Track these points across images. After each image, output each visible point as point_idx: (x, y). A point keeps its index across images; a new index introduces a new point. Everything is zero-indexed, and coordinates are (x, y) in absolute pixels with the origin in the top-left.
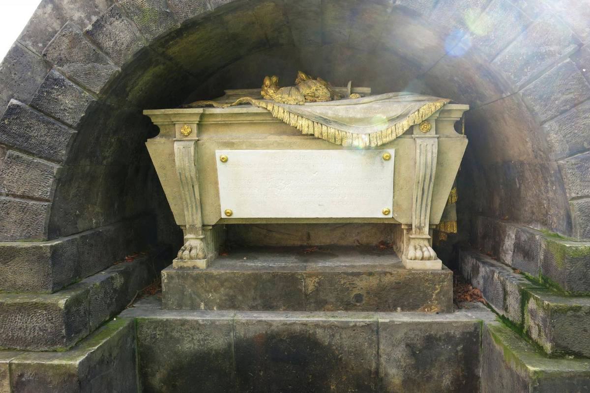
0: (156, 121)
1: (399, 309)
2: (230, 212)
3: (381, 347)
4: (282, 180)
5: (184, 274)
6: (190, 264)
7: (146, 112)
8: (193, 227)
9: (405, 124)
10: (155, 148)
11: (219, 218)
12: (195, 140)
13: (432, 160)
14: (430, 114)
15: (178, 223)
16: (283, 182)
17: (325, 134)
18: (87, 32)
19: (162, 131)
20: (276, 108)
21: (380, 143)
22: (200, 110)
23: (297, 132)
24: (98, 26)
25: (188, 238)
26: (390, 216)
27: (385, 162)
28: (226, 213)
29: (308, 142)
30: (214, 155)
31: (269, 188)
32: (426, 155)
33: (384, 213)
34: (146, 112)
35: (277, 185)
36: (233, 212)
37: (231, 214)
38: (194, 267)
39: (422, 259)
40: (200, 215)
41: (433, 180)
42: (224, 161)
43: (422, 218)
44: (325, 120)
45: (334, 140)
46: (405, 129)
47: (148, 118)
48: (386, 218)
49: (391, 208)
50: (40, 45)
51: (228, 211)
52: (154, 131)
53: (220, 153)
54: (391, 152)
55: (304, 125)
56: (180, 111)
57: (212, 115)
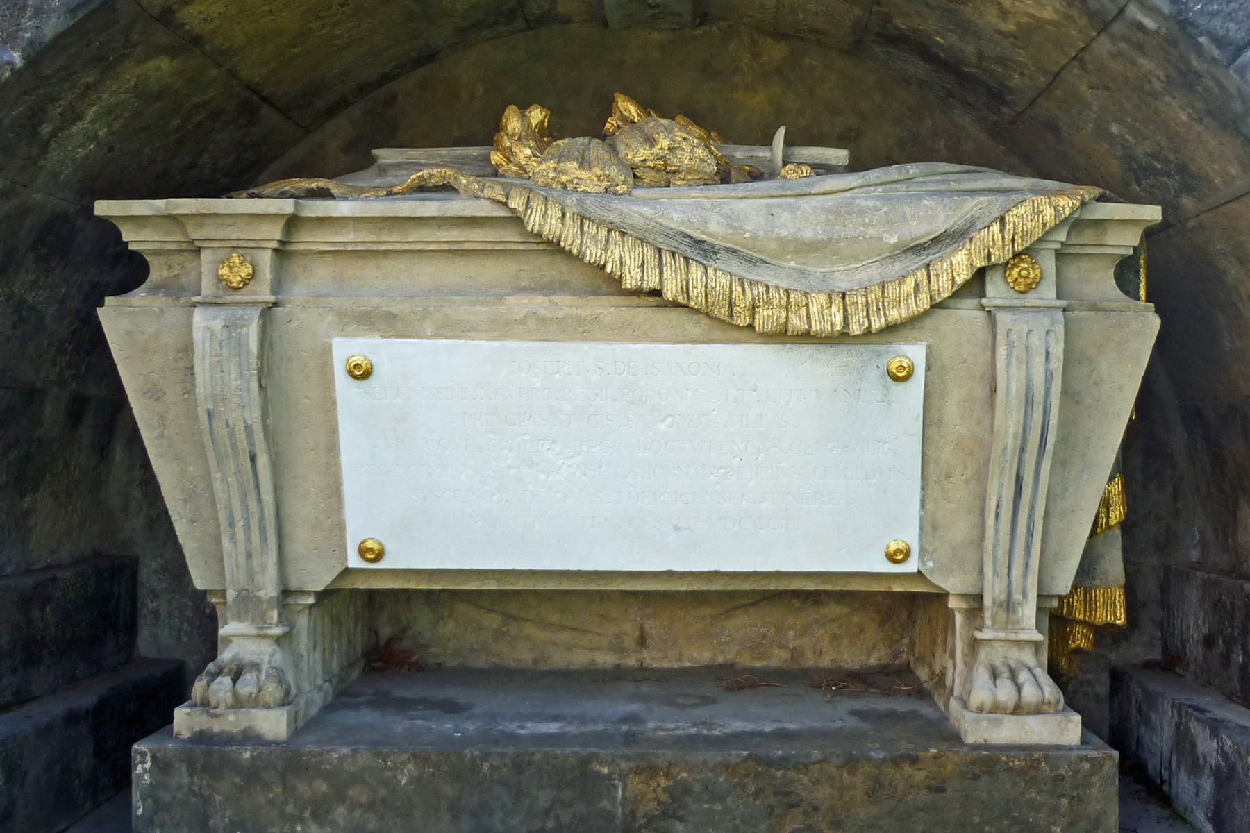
2: (376, 547)
4: (554, 442)
6: (231, 722)
7: (103, 208)
9: (961, 263)
17: (697, 291)
19: (157, 273)
21: (877, 324)
23: (613, 285)
26: (911, 566)
28: (362, 552)
30: (327, 352)
31: (510, 467)
33: (891, 558)
34: (103, 208)
36: (388, 548)
38: (249, 737)
42: (361, 373)
45: (725, 311)
47: (109, 228)
51: (369, 544)
54: (914, 352)
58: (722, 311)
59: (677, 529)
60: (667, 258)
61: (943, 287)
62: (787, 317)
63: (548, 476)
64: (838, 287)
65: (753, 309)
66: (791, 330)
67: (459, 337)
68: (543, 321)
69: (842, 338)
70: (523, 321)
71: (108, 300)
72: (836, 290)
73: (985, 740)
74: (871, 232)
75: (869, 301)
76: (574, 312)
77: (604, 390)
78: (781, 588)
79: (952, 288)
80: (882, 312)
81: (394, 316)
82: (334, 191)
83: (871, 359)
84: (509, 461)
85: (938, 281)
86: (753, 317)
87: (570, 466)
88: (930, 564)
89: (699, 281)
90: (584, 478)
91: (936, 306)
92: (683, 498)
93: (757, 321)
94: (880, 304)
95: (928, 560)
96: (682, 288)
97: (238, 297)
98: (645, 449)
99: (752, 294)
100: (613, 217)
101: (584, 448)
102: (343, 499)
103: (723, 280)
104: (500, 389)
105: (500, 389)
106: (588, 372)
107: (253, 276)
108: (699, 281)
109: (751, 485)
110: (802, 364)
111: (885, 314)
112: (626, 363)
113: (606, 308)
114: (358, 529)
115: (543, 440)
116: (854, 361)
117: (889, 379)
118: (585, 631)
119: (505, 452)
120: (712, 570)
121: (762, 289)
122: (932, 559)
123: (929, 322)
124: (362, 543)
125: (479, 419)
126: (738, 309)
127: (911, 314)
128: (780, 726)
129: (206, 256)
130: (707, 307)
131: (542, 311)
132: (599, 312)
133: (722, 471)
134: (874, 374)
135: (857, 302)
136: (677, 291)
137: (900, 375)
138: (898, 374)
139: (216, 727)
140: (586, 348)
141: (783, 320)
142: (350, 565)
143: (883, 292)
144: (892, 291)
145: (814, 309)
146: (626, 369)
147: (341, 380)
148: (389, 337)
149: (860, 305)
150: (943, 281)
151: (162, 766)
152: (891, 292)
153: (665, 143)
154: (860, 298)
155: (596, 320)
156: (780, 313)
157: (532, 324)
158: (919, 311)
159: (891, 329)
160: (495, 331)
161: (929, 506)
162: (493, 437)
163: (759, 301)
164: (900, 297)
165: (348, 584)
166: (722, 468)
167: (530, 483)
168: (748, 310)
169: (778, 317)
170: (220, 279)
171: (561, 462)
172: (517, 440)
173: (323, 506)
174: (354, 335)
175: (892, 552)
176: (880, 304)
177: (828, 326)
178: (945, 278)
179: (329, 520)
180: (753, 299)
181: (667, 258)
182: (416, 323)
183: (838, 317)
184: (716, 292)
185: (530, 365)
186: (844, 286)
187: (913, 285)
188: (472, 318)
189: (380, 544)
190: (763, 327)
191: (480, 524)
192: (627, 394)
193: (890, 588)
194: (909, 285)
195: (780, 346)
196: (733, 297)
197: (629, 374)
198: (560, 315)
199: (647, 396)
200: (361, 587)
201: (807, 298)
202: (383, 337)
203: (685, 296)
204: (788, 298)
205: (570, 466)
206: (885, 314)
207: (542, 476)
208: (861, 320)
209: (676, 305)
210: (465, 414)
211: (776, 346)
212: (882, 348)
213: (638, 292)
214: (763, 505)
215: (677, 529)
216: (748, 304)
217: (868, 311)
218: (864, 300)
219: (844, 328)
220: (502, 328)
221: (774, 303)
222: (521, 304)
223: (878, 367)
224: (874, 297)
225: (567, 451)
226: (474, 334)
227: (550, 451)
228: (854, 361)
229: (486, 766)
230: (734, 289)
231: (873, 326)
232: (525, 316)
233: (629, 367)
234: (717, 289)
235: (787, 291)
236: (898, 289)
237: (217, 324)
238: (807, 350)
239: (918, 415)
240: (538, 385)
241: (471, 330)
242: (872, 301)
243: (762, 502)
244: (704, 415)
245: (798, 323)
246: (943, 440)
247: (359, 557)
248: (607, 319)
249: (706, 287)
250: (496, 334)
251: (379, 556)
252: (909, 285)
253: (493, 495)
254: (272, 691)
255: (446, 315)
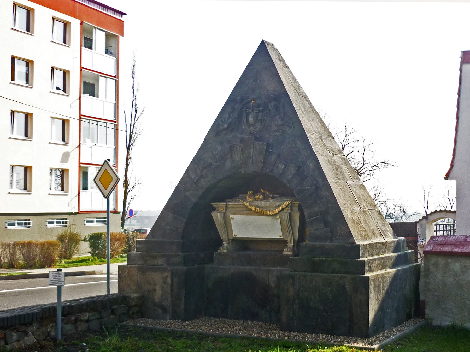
0: (215, 206)
1: (279, 266)
3: (270, 276)
5: (220, 254)
6: (222, 251)
7: (212, 203)
8: (225, 240)
9: (280, 208)
10: (214, 214)
12: (287, 206)
13: (288, 218)
14: (287, 205)
15: (222, 239)
17: (259, 211)
18: (195, 182)
19: (216, 209)
20: (246, 203)
21: (274, 214)
22: (225, 203)
23: (251, 210)
24: (198, 180)
25: (398, 322)
26: (282, 237)
27: (277, 220)
28: (235, 235)
34: (212, 203)
38: (223, 252)
39: (287, 251)
40: (227, 235)
42: (233, 219)
43: (291, 238)
44: (259, 206)
46: (280, 209)
47: (212, 205)
48: (280, 238)
50: (184, 185)
52: (214, 209)
53: (231, 216)
54: (278, 216)
55: (253, 208)
56: (220, 203)
57: (229, 204)
60: (256, 208)
69: (270, 215)
71: (212, 212)
73: (460, 57)
74: (273, 205)
82: (231, 201)
97: (222, 212)
100: (252, 204)
103: (261, 210)
107: (223, 210)
113: (251, 212)
114: (234, 233)
118: (92, 320)
121: (264, 211)
128: (246, 268)
129: (220, 208)
139: (221, 251)
144: (275, 211)
145: (268, 213)
147: (231, 220)
151: (216, 255)
153: (259, 196)
159: (275, 214)
170: (221, 210)
181: (256, 208)
194: (276, 210)
209: (257, 212)
213: (254, 211)
220: (244, 214)
222: (245, 212)
237: (220, 214)
254: (226, 248)
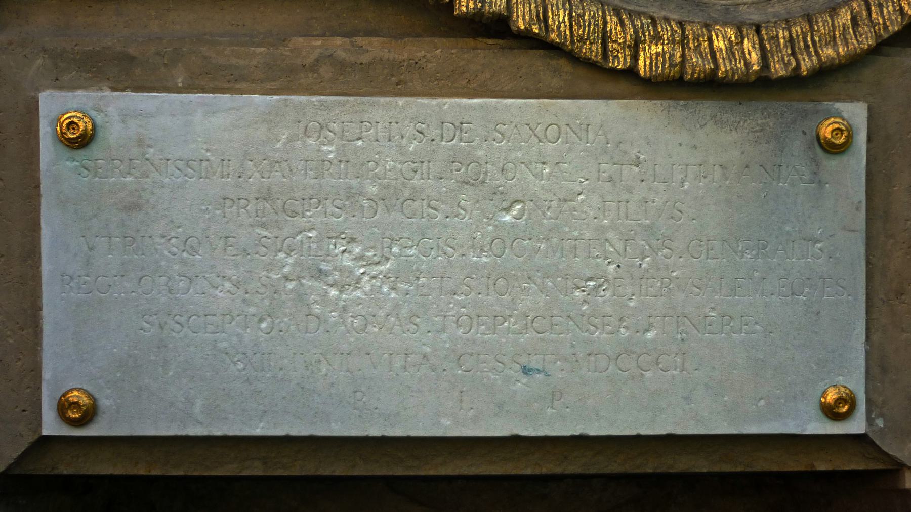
2: (84, 400)
4: (352, 240)
11: (31, 438)
16: (357, 250)
21: (807, 64)
26: (856, 426)
27: (832, 163)
28: (63, 407)
29: (623, 85)
30: (33, 110)
31: (287, 278)
32: (736, 5)
33: (831, 412)
35: (324, 266)
36: (104, 402)
37: (89, 415)
41: (649, 466)
45: (597, 48)
49: (857, 385)
51: (74, 396)
58: (594, 48)
59: (526, 371)
61: (890, 19)
62: (683, 56)
63: (341, 292)
64: (750, 19)
65: (635, 48)
66: (690, 71)
67: (223, 91)
68: (342, 67)
70: (313, 68)
72: (748, 22)
75: (794, 35)
76: (386, 55)
77: (425, 164)
78: (663, 469)
79: (902, 22)
80: (812, 49)
81: (132, 59)
83: (794, 122)
84: (286, 270)
85: (882, 12)
86: (635, 58)
87: (374, 277)
88: (880, 423)
89: (560, 7)
90: (393, 295)
91: (878, 50)
92: (534, 325)
93: (641, 62)
94: (809, 39)
95: (878, 417)
96: (538, 15)
98: (482, 250)
99: (634, 26)
101: (395, 250)
102: (42, 331)
104: (277, 162)
105: (277, 162)
106: (402, 137)
108: (560, 7)
109: (632, 304)
110: (701, 127)
111: (816, 52)
112: (457, 124)
115: (336, 238)
116: (771, 124)
117: (818, 150)
119: (281, 255)
120: (577, 433)
122: (882, 415)
123: (868, 74)
124: (64, 395)
125: (244, 208)
126: (615, 46)
127: (852, 53)
130: (572, 42)
131: (341, 54)
132: (420, 54)
133: (592, 284)
134: (797, 144)
135: (777, 36)
136: (531, 18)
137: (837, 142)
138: (833, 140)
140: (400, 103)
141: (678, 58)
142: (45, 432)
143: (811, 27)
146: (457, 133)
148: (123, 90)
149: (782, 41)
150: (889, 12)
152: (821, 24)
154: (781, 32)
155: (415, 66)
156: (673, 49)
157: (326, 71)
158: (862, 49)
160: (274, 81)
161: (875, 338)
162: (265, 233)
163: (644, 34)
164: (834, 31)
165: (44, 467)
166: (590, 279)
167: (316, 302)
168: (629, 46)
169: (671, 56)
171: (362, 270)
172: (299, 237)
173: (11, 341)
174: (72, 87)
175: (832, 402)
176: (809, 39)
177: (741, 65)
178: (891, 8)
179: (19, 363)
180: (636, 32)
182: (163, 69)
183: (753, 55)
184: (584, 21)
185: (322, 128)
186: (756, 18)
187: (849, 17)
188: (242, 62)
189: (90, 395)
190: (657, 67)
191: (240, 366)
192: (458, 170)
193: (814, 466)
194: (844, 17)
195: (671, 102)
196: (608, 29)
197: (461, 140)
198: (365, 58)
199: (486, 173)
200: (65, 472)
201: (710, 32)
202: (114, 89)
203: (542, 25)
204: (683, 31)
205: (374, 277)
206: (816, 52)
207: (333, 292)
208: (786, 59)
210: (224, 199)
211: (666, 103)
212: (810, 106)
214: (649, 335)
215: (526, 371)
216: (628, 37)
217: (793, 49)
218: (787, 34)
219: (762, 69)
221: (665, 37)
223: (804, 133)
224: (799, 31)
225: (370, 254)
226: (244, 85)
227: (346, 255)
228: (771, 124)
229: (536, 278)
230: (608, 18)
231: (803, 68)
232: (317, 60)
233: (461, 130)
234: (586, 17)
235: (681, 24)
236: (830, 21)
238: (707, 108)
239: (860, 202)
240: (331, 156)
241: (242, 78)
242: (798, 36)
243: (647, 331)
244: (565, 201)
245: (698, 63)
246: (891, 241)
247: (59, 419)
248: (430, 65)
249: (570, 15)
250: (275, 85)
251: (89, 415)
252: (844, 17)
253: (261, 320)
255: (205, 58)
